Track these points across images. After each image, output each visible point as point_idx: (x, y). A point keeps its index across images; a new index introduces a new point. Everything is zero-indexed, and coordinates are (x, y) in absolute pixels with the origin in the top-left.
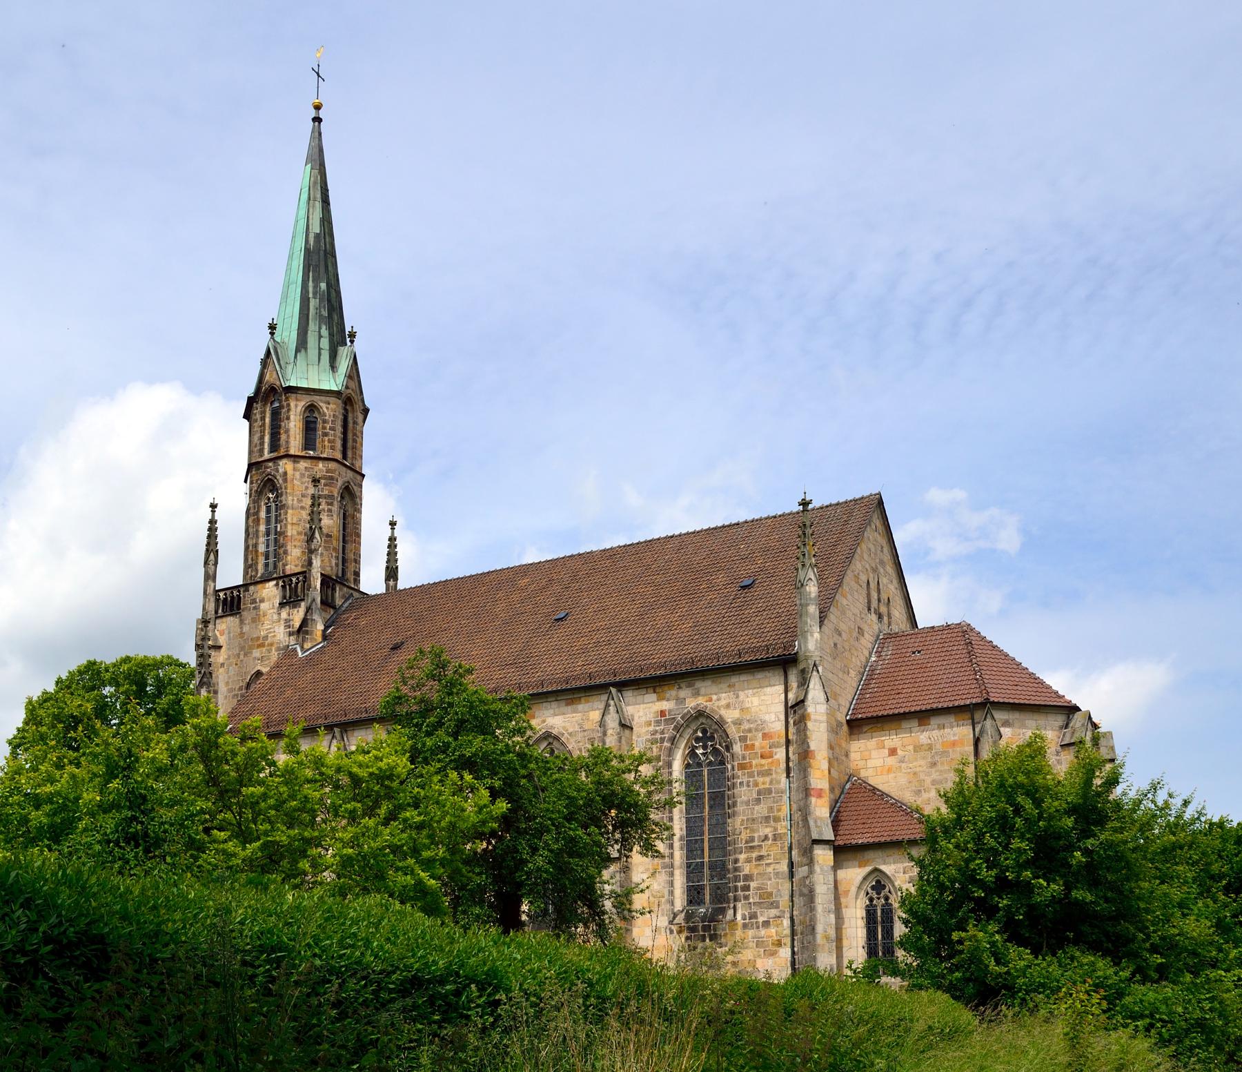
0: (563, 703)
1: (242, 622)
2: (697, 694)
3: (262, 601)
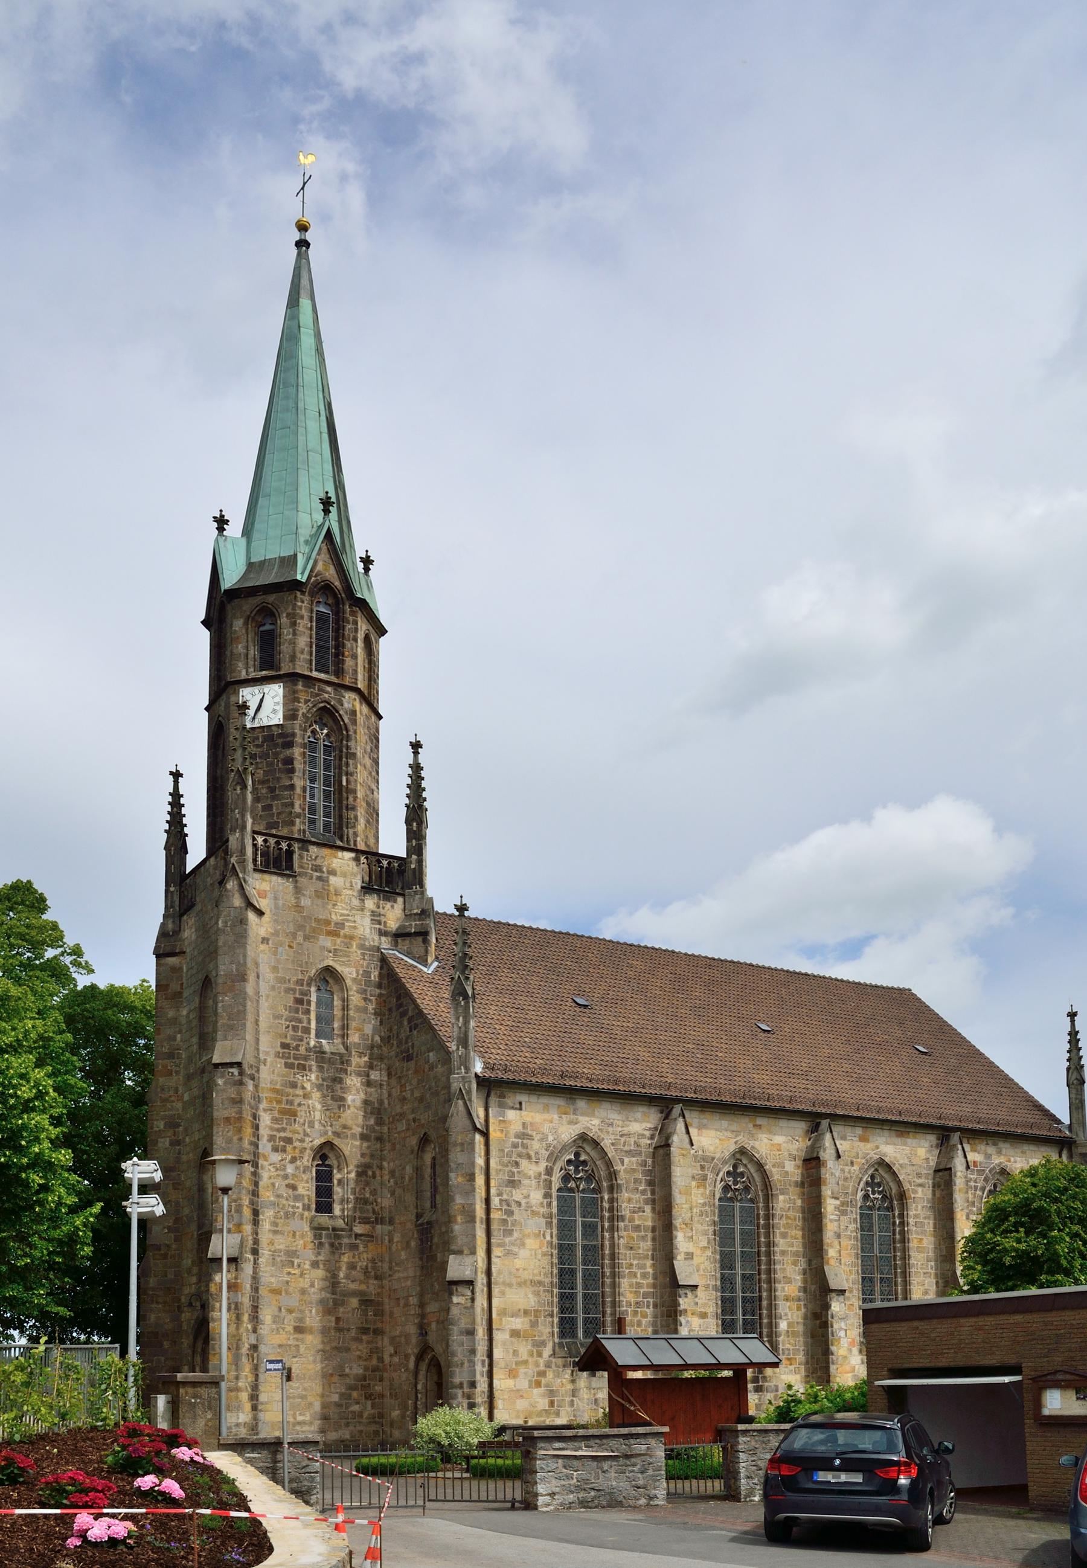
0: (893, 1133)
1: (298, 891)
2: (999, 1153)
3: (333, 872)
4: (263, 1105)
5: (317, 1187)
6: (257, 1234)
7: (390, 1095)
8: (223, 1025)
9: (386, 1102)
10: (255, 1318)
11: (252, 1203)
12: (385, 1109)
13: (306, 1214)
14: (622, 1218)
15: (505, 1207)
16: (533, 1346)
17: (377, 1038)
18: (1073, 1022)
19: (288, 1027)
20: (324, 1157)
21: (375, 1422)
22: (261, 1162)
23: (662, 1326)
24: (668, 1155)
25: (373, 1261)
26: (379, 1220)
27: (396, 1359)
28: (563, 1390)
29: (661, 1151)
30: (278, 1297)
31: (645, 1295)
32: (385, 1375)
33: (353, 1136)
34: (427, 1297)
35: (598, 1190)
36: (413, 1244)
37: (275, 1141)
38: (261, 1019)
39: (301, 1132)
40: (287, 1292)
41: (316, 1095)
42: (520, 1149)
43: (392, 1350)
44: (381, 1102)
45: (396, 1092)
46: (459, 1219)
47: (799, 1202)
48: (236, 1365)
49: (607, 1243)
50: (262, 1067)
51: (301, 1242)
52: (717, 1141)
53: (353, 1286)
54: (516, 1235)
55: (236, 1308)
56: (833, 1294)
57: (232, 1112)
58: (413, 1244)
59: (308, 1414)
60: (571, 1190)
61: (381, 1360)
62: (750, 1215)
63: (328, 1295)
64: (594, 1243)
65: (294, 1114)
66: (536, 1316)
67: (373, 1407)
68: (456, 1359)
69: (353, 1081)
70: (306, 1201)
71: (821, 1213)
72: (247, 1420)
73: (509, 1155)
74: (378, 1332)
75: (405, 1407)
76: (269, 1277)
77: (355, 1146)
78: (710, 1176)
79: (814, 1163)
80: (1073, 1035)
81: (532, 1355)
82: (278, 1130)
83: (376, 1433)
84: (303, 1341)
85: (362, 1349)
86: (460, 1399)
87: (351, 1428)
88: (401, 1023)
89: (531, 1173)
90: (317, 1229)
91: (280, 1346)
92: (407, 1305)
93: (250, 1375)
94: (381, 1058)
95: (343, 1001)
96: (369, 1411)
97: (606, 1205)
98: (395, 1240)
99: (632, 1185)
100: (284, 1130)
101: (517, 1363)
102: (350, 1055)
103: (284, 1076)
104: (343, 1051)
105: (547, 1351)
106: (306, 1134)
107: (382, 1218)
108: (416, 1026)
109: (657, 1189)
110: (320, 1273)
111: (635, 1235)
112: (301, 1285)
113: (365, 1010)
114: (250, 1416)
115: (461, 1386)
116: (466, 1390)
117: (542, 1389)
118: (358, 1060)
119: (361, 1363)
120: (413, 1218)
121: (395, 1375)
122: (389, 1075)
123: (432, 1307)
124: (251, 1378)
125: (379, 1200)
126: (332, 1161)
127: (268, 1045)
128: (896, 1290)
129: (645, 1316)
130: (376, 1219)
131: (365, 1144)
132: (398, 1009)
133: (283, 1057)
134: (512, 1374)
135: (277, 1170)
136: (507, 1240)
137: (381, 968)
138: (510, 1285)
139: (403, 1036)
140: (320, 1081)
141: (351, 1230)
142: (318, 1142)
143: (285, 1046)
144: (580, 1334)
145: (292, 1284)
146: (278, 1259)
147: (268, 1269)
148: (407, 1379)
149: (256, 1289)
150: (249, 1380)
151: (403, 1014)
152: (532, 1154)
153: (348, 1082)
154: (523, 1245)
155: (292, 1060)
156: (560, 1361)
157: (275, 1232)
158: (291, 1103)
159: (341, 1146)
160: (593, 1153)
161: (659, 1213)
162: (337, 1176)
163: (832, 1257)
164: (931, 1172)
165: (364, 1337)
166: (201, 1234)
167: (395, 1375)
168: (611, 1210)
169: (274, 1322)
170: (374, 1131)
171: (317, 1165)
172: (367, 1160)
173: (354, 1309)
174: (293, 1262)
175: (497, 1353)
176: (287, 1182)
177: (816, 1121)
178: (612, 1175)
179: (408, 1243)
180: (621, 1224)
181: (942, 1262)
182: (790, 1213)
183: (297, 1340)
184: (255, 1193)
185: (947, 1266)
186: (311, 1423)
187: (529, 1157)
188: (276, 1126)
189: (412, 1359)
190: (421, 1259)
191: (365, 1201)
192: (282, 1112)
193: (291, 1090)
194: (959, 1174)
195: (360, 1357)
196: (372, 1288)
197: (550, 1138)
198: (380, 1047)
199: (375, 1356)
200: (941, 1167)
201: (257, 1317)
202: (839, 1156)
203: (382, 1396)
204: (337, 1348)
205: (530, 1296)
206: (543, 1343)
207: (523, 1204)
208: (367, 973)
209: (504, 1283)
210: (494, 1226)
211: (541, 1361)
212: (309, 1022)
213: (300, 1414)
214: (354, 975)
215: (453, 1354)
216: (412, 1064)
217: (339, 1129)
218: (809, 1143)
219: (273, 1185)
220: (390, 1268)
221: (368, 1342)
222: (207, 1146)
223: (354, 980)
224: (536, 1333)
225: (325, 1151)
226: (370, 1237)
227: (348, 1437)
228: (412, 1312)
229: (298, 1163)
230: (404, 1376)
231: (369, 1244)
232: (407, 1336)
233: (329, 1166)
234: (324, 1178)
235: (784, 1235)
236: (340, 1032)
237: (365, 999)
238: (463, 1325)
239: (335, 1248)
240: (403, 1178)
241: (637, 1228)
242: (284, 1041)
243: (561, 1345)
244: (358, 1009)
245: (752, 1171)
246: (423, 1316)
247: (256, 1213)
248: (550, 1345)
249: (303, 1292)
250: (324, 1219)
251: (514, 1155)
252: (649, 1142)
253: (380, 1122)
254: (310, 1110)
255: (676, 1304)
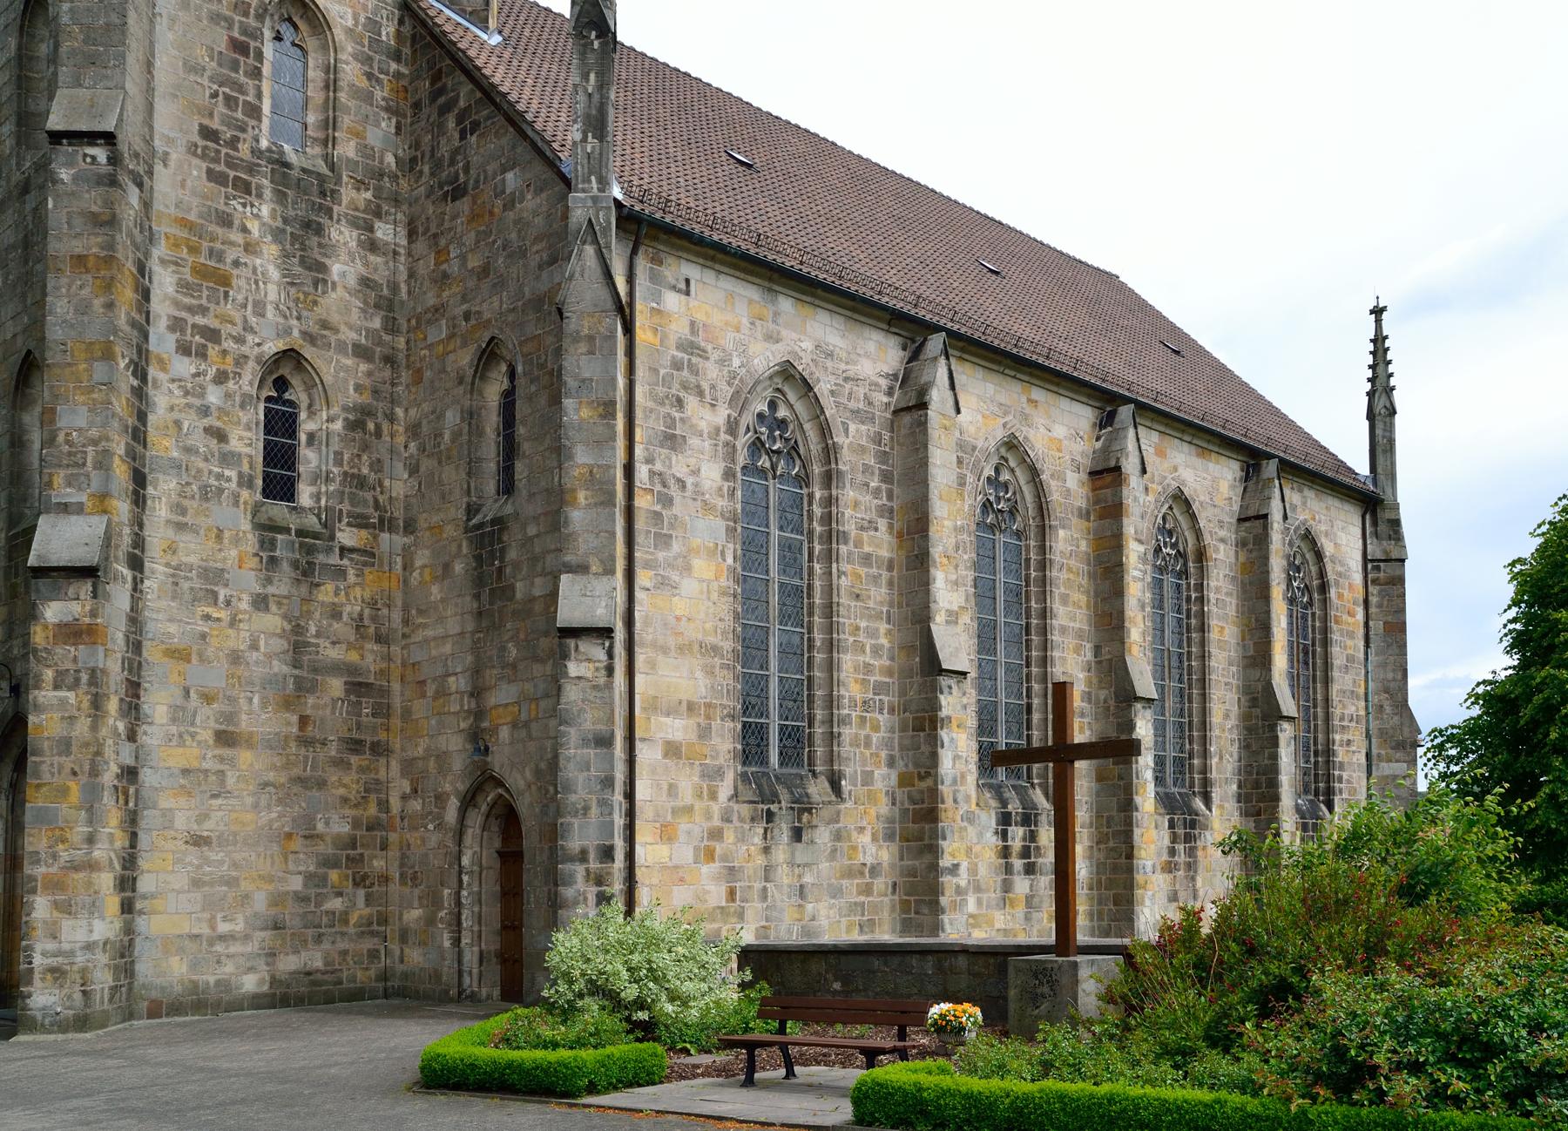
4: (160, 251)
5: (267, 444)
6: (141, 526)
7: (412, 275)
8: (73, 52)
9: (404, 288)
10: (133, 709)
11: (132, 455)
12: (402, 303)
13: (245, 494)
14: (843, 537)
15: (658, 488)
16: (703, 776)
17: (390, 159)
18: (1378, 322)
19: (215, 95)
20: (281, 384)
21: (373, 934)
22: (153, 372)
23: (901, 749)
24: (923, 424)
25: (373, 604)
26: (387, 524)
27: (416, 805)
28: (749, 868)
29: (907, 419)
30: (182, 666)
31: (879, 688)
32: (393, 837)
33: (341, 347)
34: (491, 675)
35: (803, 480)
36: (458, 567)
37: (183, 331)
38: (158, 63)
39: (239, 321)
40: (202, 659)
41: (271, 250)
42: (685, 373)
43: (406, 786)
44: (394, 287)
45: (426, 267)
46: (582, 496)
47: (1083, 546)
48: (90, 810)
49: (817, 583)
50: (158, 168)
51: (234, 553)
52: (979, 417)
53: (334, 653)
54: (676, 547)
55: (93, 681)
56: (1139, 706)
57: (91, 244)
58: (458, 567)
59: (240, 918)
60: (762, 473)
61: (384, 805)
62: (1018, 562)
63: (286, 669)
64: (797, 582)
65: (225, 281)
66: (708, 717)
67: (369, 900)
68: (573, 798)
69: (343, 235)
70: (246, 468)
71: (1121, 564)
72: (111, 935)
73: (667, 382)
74: (379, 750)
75: (434, 901)
76: (167, 621)
77: (347, 369)
78: (970, 479)
79: (1108, 478)
80: (1379, 341)
81: (700, 796)
82: (190, 309)
83: (373, 955)
84: (232, 762)
85: (346, 783)
86: (580, 884)
87: (326, 946)
88: (441, 126)
89: (703, 425)
90: (268, 530)
91: (186, 772)
92: (442, 693)
93: (119, 834)
94: (396, 201)
95: (327, 72)
96: (361, 910)
97: (818, 511)
98: (418, 563)
99: (860, 478)
100: (204, 311)
101: (675, 811)
102: (338, 181)
103: (205, 197)
104: (325, 170)
105: (725, 789)
106: (248, 328)
107: (391, 520)
108: (475, 126)
109: (896, 491)
110: (272, 621)
111: (863, 571)
112: (231, 644)
113: (368, 98)
114: (118, 925)
115: (583, 856)
116: (594, 865)
117: (715, 867)
118: (354, 193)
119: (347, 812)
120: (461, 514)
121: (413, 837)
122: (412, 234)
123: (502, 695)
124: (121, 841)
125: (387, 483)
126: (297, 393)
127: (172, 126)
128: (1190, 709)
129: (876, 728)
130: (381, 520)
131: (363, 367)
132: (433, 99)
133: (204, 157)
134: (667, 834)
135: (187, 393)
136: (661, 555)
137: (401, 22)
138: (665, 650)
139: (444, 151)
140: (279, 223)
141: (332, 538)
142: (272, 347)
143: (208, 133)
144: (774, 758)
145: (214, 642)
146: (186, 585)
147: (163, 604)
148: (441, 845)
149: (136, 646)
150: (118, 844)
151: (444, 110)
152: (705, 386)
153: (334, 234)
154: (687, 569)
155: (222, 168)
156: (745, 810)
157: (181, 527)
158: (220, 257)
159: (318, 363)
160: (800, 407)
161: (900, 536)
162: (306, 425)
163: (1135, 642)
164: (1234, 521)
165: (354, 759)
166: (16, 536)
167: (413, 837)
168: (827, 519)
169: (174, 720)
170: (380, 343)
171: (269, 399)
172: (366, 399)
173: (334, 701)
174: (215, 595)
175: (642, 791)
176: (206, 422)
177: (1107, 403)
178: (830, 452)
179: (447, 567)
180: (843, 549)
181: (1245, 667)
182: (1072, 562)
183: (222, 759)
184: (139, 435)
185: (1256, 673)
186: (247, 938)
187: (701, 394)
188: (187, 300)
189: (453, 804)
190: (477, 597)
191: (361, 482)
192: (201, 272)
193: (220, 231)
194: (1276, 526)
195: (345, 800)
196: (370, 658)
197: (736, 362)
198: (394, 178)
199: (373, 797)
200: (1251, 513)
201: (137, 708)
202: (1144, 471)
203: (385, 879)
204: (301, 781)
205: (699, 674)
206: (719, 773)
207: (689, 486)
208: (373, 25)
209: (654, 645)
210: (640, 524)
211: (716, 809)
212: (259, 96)
213: (225, 919)
214: (350, 23)
215: (568, 789)
216: (464, 205)
217: (315, 329)
218: (1099, 445)
219: (178, 424)
220: (406, 622)
221: (361, 770)
222: (32, 345)
223: (349, 32)
224: (706, 751)
225: (285, 371)
226: (367, 555)
227: (319, 964)
228: (455, 708)
229: (231, 384)
230: (434, 839)
231: (367, 570)
232: (442, 757)
233: (291, 404)
234: (280, 426)
235: (1065, 600)
236: (321, 135)
237: (370, 76)
238: (588, 725)
239: (306, 572)
240: (438, 435)
241: (867, 559)
242: (206, 122)
243: (744, 776)
244: (356, 92)
245: (1022, 482)
246: (479, 714)
247: (139, 479)
248: (730, 777)
249: (236, 658)
250: (278, 510)
251: (676, 386)
252: (885, 399)
253: (391, 326)
254: (257, 278)
255: (935, 706)
